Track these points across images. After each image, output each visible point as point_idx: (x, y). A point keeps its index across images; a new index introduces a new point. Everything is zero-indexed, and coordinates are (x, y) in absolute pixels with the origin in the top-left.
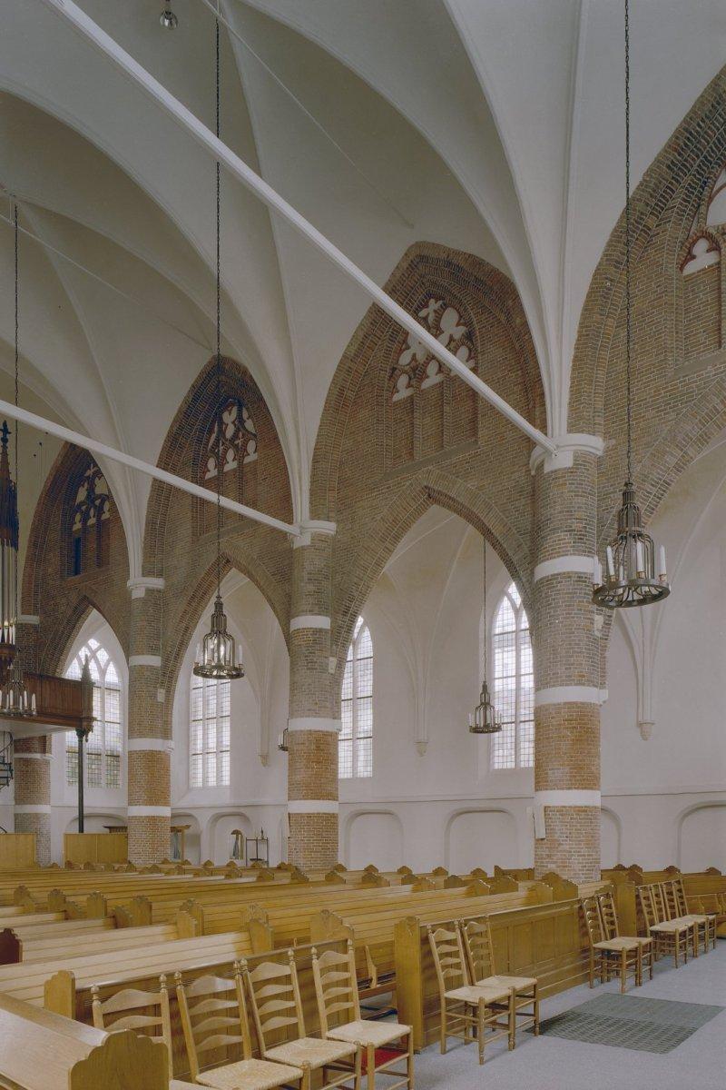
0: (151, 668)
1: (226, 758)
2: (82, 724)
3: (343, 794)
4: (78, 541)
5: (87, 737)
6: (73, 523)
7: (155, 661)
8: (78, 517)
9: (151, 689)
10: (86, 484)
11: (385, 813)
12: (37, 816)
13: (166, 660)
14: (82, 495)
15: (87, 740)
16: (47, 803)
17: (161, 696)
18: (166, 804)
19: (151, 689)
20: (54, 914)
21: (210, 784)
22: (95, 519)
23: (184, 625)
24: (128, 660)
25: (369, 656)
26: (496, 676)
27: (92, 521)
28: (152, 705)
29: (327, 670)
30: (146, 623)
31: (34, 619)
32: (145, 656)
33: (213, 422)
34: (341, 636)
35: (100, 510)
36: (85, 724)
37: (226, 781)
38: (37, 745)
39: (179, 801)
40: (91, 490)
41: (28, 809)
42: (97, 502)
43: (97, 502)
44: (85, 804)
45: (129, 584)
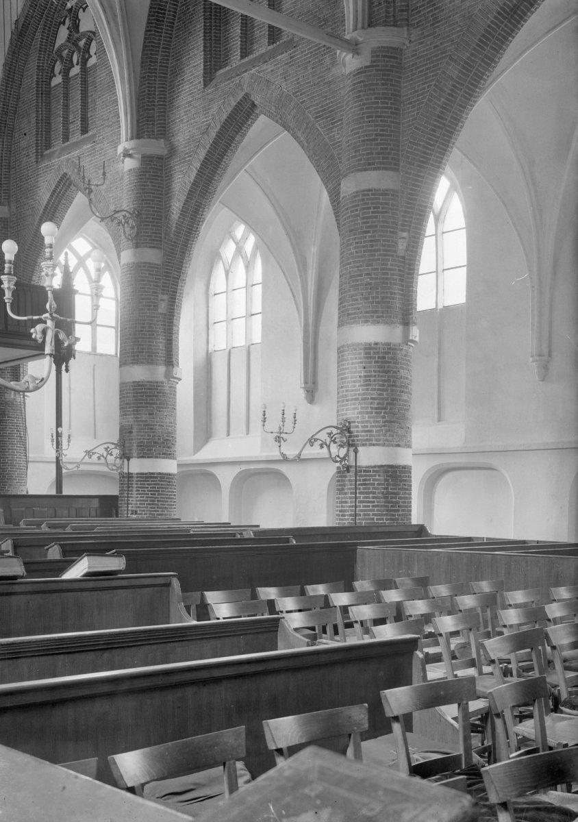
5: (67, 364)
6: (53, 75)
8: (58, 67)
10: (67, 20)
11: (473, 468)
14: (63, 33)
15: (67, 370)
17: (163, 307)
18: (169, 455)
22: (79, 67)
27: (76, 70)
29: (396, 252)
40: (75, 26)
42: (82, 43)
43: (82, 43)
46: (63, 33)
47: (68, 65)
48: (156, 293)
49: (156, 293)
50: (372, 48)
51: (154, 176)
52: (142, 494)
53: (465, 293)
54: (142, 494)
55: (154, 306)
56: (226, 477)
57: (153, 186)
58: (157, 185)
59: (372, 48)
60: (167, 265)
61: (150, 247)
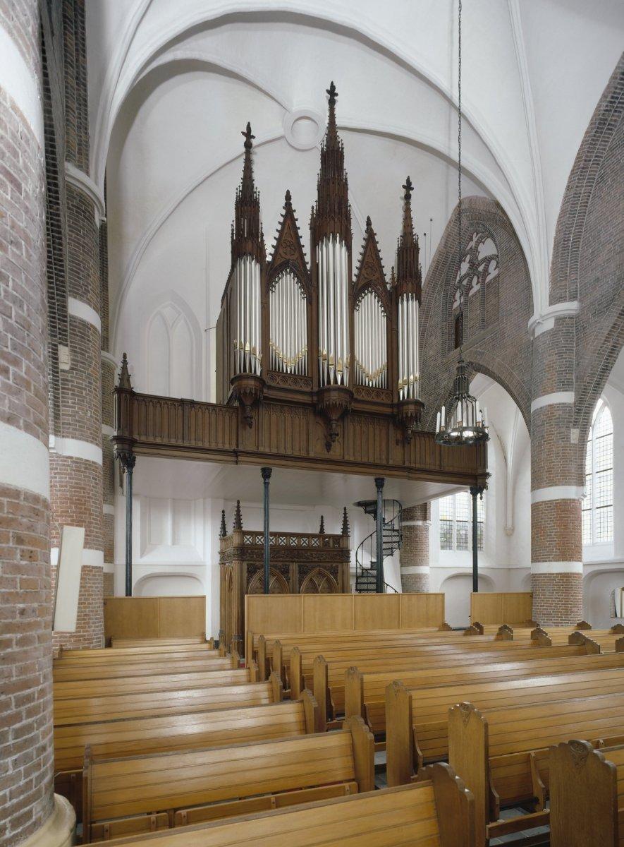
0: (563, 406)
2: (476, 482)
3: (587, 556)
9: (563, 430)
16: (427, 565)
17: (575, 434)
23: (609, 345)
25: (609, 432)
26: (587, 472)
28: (564, 448)
30: (554, 357)
34: (581, 416)
36: (480, 481)
38: (419, 513)
41: (411, 570)
42: (481, 269)
46: (465, 267)
48: (568, 427)
49: (568, 427)
61: (563, 391)
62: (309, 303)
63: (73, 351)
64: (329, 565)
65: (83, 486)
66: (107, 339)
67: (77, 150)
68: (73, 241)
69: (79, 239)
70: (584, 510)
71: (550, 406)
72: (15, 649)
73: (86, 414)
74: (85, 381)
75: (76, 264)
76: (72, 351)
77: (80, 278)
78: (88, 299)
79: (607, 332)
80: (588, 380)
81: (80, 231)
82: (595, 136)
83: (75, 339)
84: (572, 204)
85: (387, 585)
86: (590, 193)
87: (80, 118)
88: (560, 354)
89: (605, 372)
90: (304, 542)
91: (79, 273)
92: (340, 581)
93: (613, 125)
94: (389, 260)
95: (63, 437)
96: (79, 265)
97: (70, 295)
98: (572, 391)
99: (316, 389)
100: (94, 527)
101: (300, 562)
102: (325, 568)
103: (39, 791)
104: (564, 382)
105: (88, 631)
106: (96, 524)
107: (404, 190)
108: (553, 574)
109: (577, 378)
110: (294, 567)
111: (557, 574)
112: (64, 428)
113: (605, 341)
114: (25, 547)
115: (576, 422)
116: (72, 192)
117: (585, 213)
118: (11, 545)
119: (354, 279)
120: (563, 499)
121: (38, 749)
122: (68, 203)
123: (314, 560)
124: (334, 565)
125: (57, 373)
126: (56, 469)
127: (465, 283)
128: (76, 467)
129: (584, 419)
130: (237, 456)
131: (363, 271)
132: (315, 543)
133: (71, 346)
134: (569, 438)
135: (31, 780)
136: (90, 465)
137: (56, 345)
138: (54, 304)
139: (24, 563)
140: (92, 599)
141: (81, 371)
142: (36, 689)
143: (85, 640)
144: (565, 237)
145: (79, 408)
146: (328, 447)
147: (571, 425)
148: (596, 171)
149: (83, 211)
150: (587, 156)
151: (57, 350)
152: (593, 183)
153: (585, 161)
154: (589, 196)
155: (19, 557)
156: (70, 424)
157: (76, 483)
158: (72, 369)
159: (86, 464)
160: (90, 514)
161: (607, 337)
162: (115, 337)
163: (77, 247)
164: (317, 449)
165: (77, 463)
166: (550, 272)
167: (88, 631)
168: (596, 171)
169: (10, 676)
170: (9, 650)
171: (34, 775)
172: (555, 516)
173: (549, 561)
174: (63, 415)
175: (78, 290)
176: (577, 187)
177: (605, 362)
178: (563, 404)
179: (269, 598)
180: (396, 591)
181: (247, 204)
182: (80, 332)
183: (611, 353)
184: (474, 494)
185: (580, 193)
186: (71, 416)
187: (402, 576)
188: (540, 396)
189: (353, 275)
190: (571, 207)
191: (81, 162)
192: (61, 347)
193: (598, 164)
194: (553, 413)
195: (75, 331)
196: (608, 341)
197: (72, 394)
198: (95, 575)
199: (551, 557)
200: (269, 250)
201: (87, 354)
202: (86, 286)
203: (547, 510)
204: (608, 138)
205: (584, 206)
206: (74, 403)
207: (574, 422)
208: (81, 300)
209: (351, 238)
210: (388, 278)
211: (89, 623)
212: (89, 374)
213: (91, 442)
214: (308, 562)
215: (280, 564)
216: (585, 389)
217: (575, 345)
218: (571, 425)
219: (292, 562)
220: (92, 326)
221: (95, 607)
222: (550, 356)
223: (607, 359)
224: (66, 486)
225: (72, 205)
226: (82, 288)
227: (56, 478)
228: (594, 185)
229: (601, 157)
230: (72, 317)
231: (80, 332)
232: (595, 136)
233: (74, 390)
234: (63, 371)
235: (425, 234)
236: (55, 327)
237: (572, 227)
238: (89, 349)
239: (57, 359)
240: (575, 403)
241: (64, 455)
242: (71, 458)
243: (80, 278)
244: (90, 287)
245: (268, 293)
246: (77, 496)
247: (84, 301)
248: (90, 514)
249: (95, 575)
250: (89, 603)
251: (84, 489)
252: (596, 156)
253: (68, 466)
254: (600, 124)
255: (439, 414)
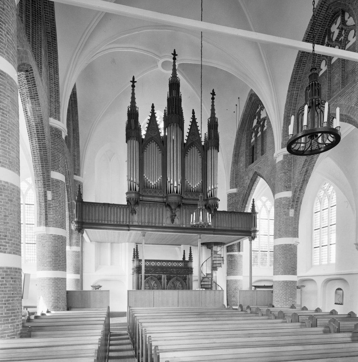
0: (286, 198)
1: (333, 248)
4: (253, 148)
7: (288, 194)
9: (286, 210)
12: (236, 281)
13: (295, 192)
19: (286, 210)
20: (282, 320)
21: (323, 263)
23: (305, 169)
24: (274, 196)
30: (283, 174)
31: (234, 190)
32: (283, 192)
33: (325, 37)
35: (263, 126)
36: (253, 234)
37: (333, 260)
38: (236, 248)
39: (302, 271)
41: (232, 278)
42: (261, 123)
44: (253, 275)
45: (275, 155)
46: (255, 121)
47: (257, 132)
48: (288, 209)
49: (288, 209)
50: (38, 226)
51: (289, 162)
52: (282, 289)
53: (114, 356)
54: (282, 289)
55: (288, 214)
56: (320, 281)
57: (288, 166)
58: (290, 166)
59: (39, 224)
60: (293, 197)
61: (286, 191)
62: (163, 155)
63: (53, 192)
64: (182, 275)
65: (57, 246)
66: (79, 169)
67: (54, 111)
68: (53, 148)
69: (55, 147)
70: (335, 244)
71: (280, 198)
72: (11, 302)
73: (58, 217)
74: (58, 203)
75: (54, 157)
76: (52, 192)
77: (55, 163)
78: (59, 170)
79: (303, 163)
80: (296, 186)
81: (55, 144)
82: (297, 67)
83: (53, 187)
84: (290, 99)
85: (218, 285)
86: (298, 94)
87: (56, 98)
88: (285, 173)
89: (304, 182)
90: (175, 264)
91: (55, 161)
92: (187, 283)
93: (305, 63)
94: (204, 131)
95: (49, 226)
96: (55, 157)
97: (51, 170)
98: (291, 191)
99: (165, 195)
100: (62, 262)
101: (167, 274)
102: (180, 277)
103: (17, 334)
104: (287, 186)
105: (59, 304)
106: (63, 260)
107: (212, 95)
108: (280, 281)
109: (293, 184)
110: (164, 276)
111: (282, 281)
112: (49, 223)
113: (302, 167)
114: (13, 280)
115: (293, 206)
116: (53, 128)
117: (296, 103)
118: (10, 279)
119: (185, 142)
120: (285, 244)
121: (16, 325)
122: (51, 133)
123: (174, 273)
124: (185, 275)
125: (47, 201)
126: (46, 239)
127: (255, 129)
128: (54, 238)
129: (296, 205)
130: (129, 227)
131: (190, 137)
132: (181, 265)
133: (52, 190)
134: (288, 214)
135: (15, 331)
136: (60, 237)
137: (46, 191)
138: (45, 176)
139: (13, 283)
140: (61, 291)
141: (56, 200)
142: (16, 311)
143: (58, 307)
144: (287, 115)
145: (55, 215)
146: (173, 221)
147: (290, 207)
148: (300, 84)
149: (57, 135)
150: (295, 77)
151: (46, 193)
152: (299, 89)
153: (294, 79)
154: (298, 95)
155: (12, 282)
156: (52, 221)
157: (54, 245)
158: (52, 199)
159: (58, 237)
160: (60, 257)
161: (303, 166)
162: (83, 166)
163: (55, 150)
164: (167, 222)
165: (55, 237)
166: (282, 132)
167: (59, 304)
168: (300, 84)
169: (10, 307)
170: (9, 302)
171: (15, 330)
172: (281, 252)
173: (279, 275)
174: (49, 218)
175: (55, 167)
176: (292, 91)
177: (303, 177)
178: (286, 197)
179: (184, 292)
180: (222, 289)
181: (133, 114)
182: (55, 184)
183: (306, 173)
184: (251, 241)
185: (293, 94)
186: (52, 218)
187: (227, 281)
188: (277, 193)
189: (184, 140)
190: (290, 101)
191: (56, 116)
192: (48, 192)
193: (300, 80)
194: (281, 202)
195: (54, 184)
196: (304, 168)
197: (53, 210)
198: (62, 281)
199: (279, 272)
200: (143, 132)
201: (58, 193)
202: (58, 165)
203: (278, 249)
204: (304, 68)
205: (295, 100)
206: (53, 213)
207: (292, 206)
208: (56, 171)
209: (184, 123)
210: (203, 139)
211: (59, 301)
212: (59, 200)
213: (61, 228)
214: (172, 274)
215: (157, 275)
216: (295, 190)
217: (292, 168)
218: (290, 207)
219: (163, 274)
220: (60, 181)
221: (62, 294)
222: (281, 174)
223: (304, 176)
224: (50, 246)
225: (53, 134)
226: (56, 166)
227: (46, 243)
228: (300, 90)
229: (302, 77)
230: (52, 179)
231: (55, 184)
232: (297, 67)
233: (53, 208)
234: (49, 201)
235: (236, 105)
236: (45, 184)
237: (291, 110)
238: (59, 190)
239: (46, 196)
240: (292, 197)
241: (49, 234)
242: (52, 235)
243: (55, 163)
244: (60, 165)
245: (143, 152)
246: (55, 250)
247: (58, 172)
248: (60, 257)
249: (62, 281)
250: (59, 293)
251: (57, 247)
252: (299, 77)
253: (51, 238)
254: (299, 62)
255: (192, 215)
